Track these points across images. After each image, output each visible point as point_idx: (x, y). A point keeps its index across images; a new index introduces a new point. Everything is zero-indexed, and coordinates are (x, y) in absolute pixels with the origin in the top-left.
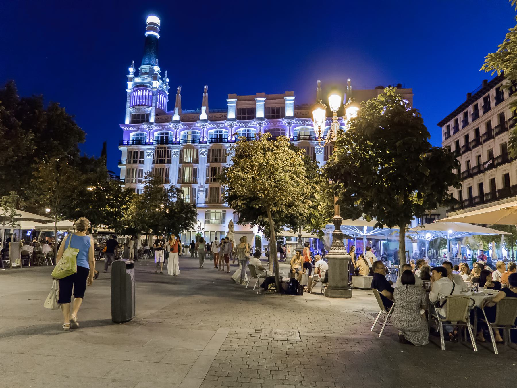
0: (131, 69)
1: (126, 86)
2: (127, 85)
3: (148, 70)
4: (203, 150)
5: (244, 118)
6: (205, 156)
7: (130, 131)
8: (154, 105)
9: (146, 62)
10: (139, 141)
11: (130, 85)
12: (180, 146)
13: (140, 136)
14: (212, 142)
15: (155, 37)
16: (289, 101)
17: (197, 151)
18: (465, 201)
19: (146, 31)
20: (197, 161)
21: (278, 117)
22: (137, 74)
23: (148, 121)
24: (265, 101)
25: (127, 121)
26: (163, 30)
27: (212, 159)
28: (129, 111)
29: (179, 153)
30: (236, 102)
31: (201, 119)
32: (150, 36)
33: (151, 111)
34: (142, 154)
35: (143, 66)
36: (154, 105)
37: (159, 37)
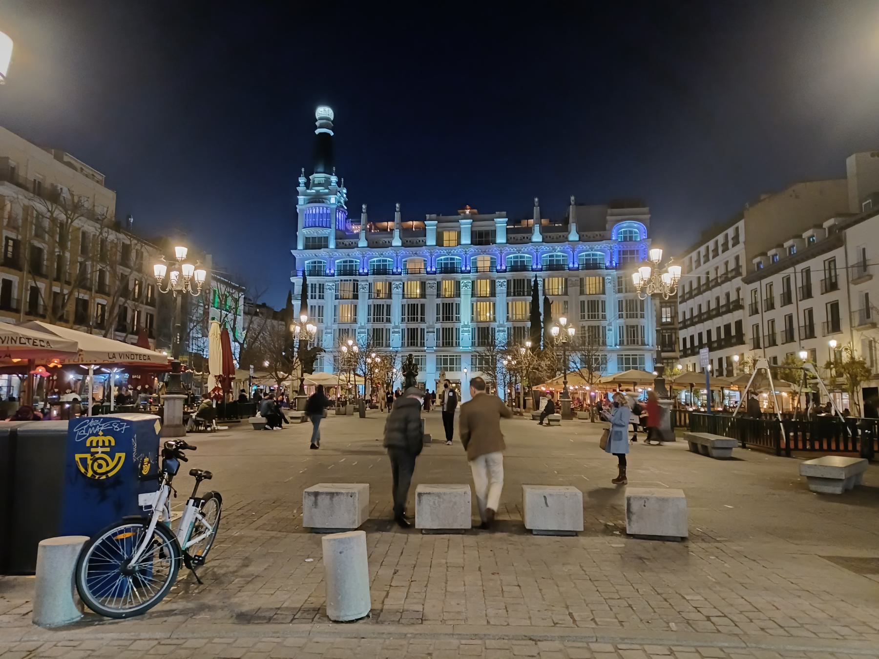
0: (302, 180)
1: (296, 202)
2: (297, 200)
3: (322, 180)
4: (574, 279)
5: (480, 243)
6: (504, 288)
7: (303, 256)
8: (333, 226)
9: (319, 170)
10: (316, 271)
11: (301, 199)
12: (472, 276)
13: (591, 257)
14: (374, 274)
15: (329, 134)
16: (431, 225)
17: (604, 279)
18: (714, 342)
19: (316, 128)
20: (493, 294)
21: (487, 243)
22: (307, 185)
23: (327, 247)
24: (471, 224)
25: (300, 246)
26: (335, 125)
27: (514, 292)
28: (303, 233)
29: (470, 284)
30: (436, 225)
31: (393, 244)
32: (320, 134)
33: (329, 234)
34: (322, 287)
35: (315, 175)
36: (333, 226)
37: (332, 134)
